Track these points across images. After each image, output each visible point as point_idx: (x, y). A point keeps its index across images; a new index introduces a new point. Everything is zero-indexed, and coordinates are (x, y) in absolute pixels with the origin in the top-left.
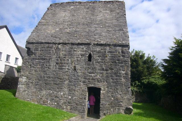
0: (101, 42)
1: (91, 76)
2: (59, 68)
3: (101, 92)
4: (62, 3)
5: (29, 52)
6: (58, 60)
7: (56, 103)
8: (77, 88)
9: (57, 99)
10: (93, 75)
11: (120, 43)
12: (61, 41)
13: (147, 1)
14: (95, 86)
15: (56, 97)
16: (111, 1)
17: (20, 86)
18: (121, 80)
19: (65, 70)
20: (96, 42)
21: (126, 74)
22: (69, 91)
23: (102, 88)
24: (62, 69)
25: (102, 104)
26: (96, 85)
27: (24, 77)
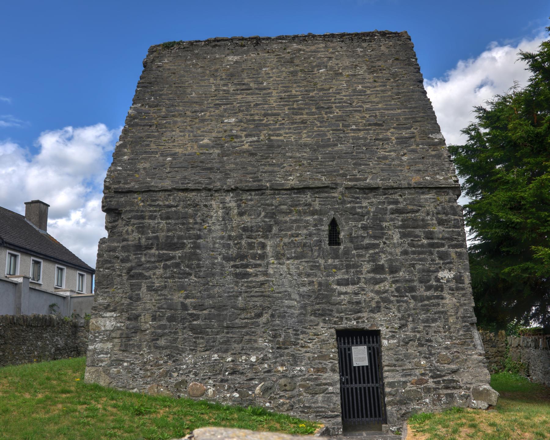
0: (366, 179)
1: (346, 293)
2: (236, 274)
3: (385, 342)
4: (191, 43)
5: (116, 223)
6: (228, 247)
7: (236, 395)
8: (301, 336)
9: (239, 379)
10: (350, 289)
11: (431, 183)
12: (230, 182)
13: (47, 131)
14: (361, 326)
15: (234, 372)
16: (364, 34)
17: (99, 346)
18: (444, 301)
19: (253, 279)
20: (350, 180)
21: (458, 279)
22: (278, 348)
23: (383, 330)
24: (246, 275)
25: (391, 385)
26: (364, 322)
27: (108, 314)
